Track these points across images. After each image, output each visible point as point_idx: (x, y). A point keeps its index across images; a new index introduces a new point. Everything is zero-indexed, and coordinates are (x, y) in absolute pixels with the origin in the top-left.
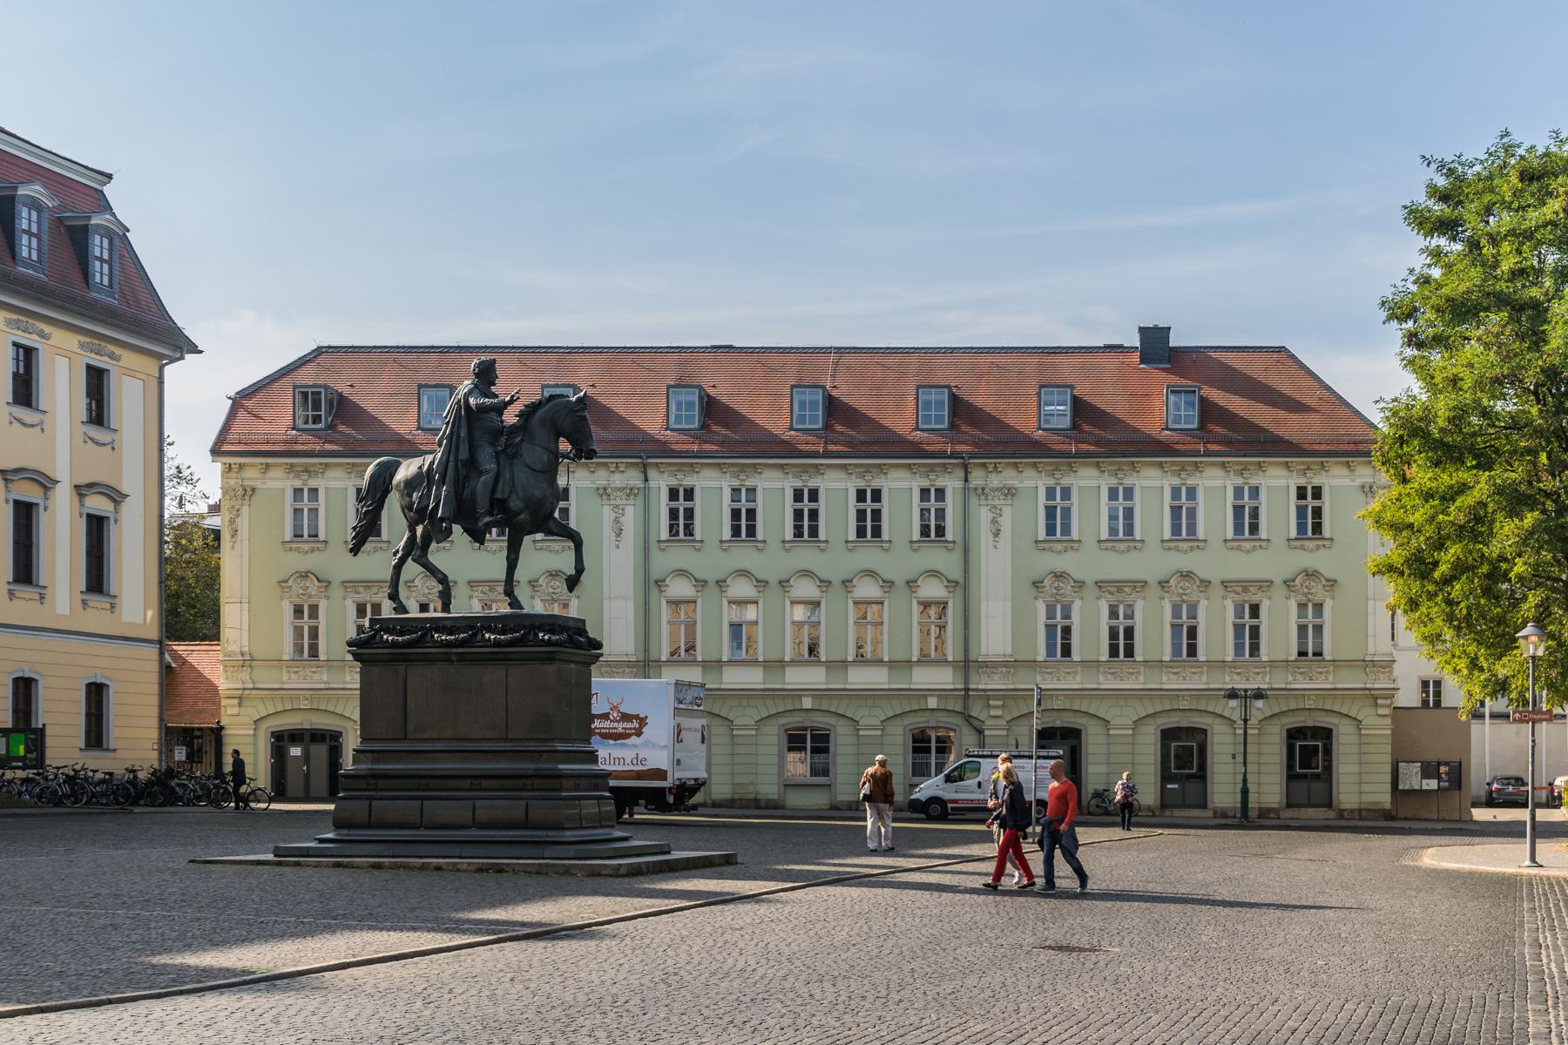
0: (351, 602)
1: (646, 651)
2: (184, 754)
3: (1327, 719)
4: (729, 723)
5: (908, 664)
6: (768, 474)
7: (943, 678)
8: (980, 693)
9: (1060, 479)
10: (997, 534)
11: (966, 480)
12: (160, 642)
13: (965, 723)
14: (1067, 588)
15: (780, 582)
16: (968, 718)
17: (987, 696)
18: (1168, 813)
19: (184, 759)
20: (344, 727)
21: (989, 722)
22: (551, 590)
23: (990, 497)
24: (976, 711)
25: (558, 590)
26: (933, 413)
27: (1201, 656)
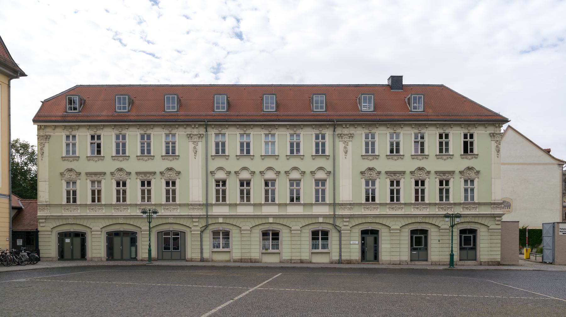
0: (89, 181)
1: (207, 200)
2: (21, 242)
3: (377, 226)
4: (240, 229)
5: (261, 205)
6: (81, 130)
7: (325, 210)
8: (189, 216)
9: (420, 130)
10: (346, 152)
11: (334, 131)
12: (9, 196)
13: (334, 228)
14: (374, 174)
15: (260, 172)
16: (335, 226)
17: (342, 217)
18: (413, 263)
19: (21, 244)
20: (87, 231)
21: (343, 228)
22: (169, 176)
23: (343, 138)
24: (339, 223)
25: (172, 176)
26: (319, 105)
27: (78, 202)
